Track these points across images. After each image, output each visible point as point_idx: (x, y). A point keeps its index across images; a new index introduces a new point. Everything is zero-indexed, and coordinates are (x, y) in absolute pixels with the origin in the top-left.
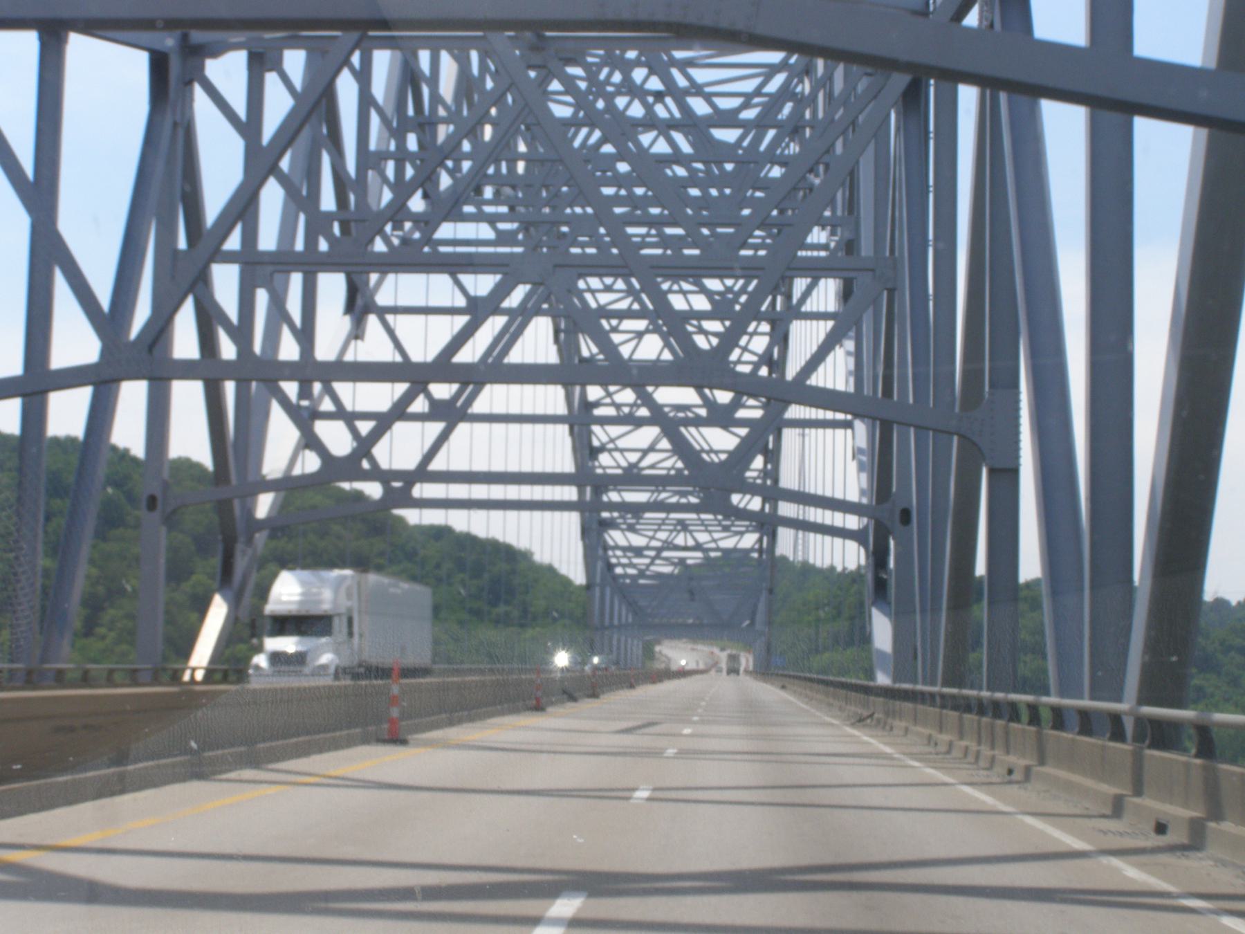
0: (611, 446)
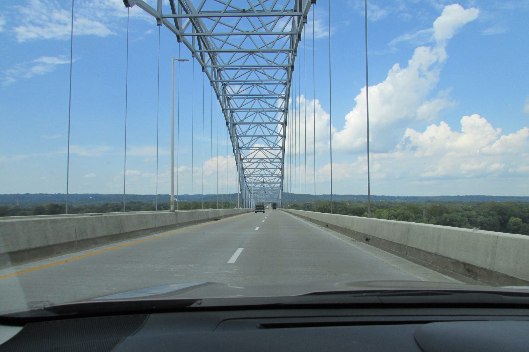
0: (246, 158)
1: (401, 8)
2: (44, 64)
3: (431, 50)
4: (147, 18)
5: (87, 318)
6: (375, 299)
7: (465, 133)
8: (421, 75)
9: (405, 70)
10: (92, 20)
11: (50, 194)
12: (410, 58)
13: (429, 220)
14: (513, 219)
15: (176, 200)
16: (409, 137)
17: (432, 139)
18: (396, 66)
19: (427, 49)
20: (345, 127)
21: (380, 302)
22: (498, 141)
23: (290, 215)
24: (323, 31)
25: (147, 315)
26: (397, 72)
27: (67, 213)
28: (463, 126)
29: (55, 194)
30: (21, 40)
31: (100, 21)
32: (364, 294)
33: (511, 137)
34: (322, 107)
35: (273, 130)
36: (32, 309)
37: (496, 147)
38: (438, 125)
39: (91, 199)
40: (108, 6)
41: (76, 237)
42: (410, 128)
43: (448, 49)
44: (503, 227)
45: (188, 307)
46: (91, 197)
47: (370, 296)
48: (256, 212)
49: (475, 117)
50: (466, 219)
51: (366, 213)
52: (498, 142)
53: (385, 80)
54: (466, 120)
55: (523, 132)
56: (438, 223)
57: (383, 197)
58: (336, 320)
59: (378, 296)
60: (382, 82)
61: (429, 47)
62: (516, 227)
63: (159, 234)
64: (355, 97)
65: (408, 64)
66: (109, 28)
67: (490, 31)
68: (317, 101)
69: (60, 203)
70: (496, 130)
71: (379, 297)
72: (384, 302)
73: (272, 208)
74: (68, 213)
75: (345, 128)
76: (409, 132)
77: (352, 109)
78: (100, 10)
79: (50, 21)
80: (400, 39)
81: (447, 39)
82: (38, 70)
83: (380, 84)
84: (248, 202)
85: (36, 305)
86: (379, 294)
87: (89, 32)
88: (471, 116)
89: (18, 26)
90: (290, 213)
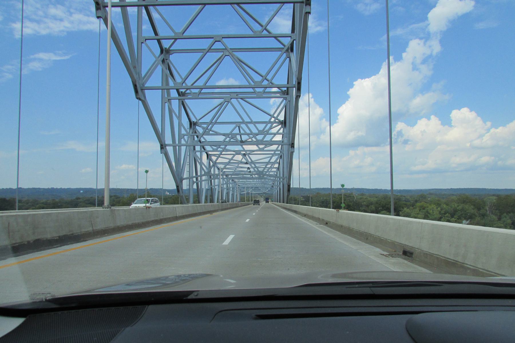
2: (40, 60)
3: (425, 44)
5: (88, 310)
6: (367, 291)
7: (455, 127)
8: (415, 68)
10: (88, 16)
12: (404, 51)
15: (167, 194)
16: (401, 130)
17: (423, 132)
20: (337, 121)
21: (372, 293)
22: (488, 134)
23: (292, 215)
25: (145, 307)
27: (17, 208)
32: (357, 286)
33: (500, 130)
34: (314, 101)
35: (264, 74)
36: (34, 301)
37: (487, 140)
38: (429, 119)
42: (401, 122)
43: (442, 42)
44: (471, 219)
45: (185, 298)
46: (81, 191)
47: (363, 287)
48: (254, 205)
53: (378, 73)
54: (456, 114)
58: (329, 311)
59: (370, 287)
61: (423, 41)
63: (60, 248)
64: (349, 90)
65: (402, 57)
67: (481, 26)
68: (311, 96)
69: (8, 197)
70: (485, 124)
71: (371, 288)
72: (376, 293)
73: (265, 201)
74: (19, 210)
75: (338, 122)
77: (344, 103)
79: (46, 16)
81: (441, 31)
83: (373, 77)
84: (233, 195)
85: (38, 297)
86: (371, 285)
87: (85, 28)
90: (295, 212)
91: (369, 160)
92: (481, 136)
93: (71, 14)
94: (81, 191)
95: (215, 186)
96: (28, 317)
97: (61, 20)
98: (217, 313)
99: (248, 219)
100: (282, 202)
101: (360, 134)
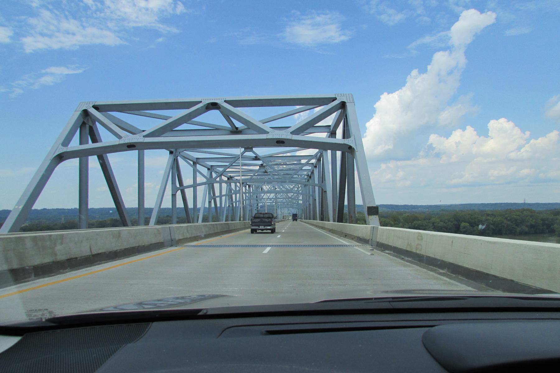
1: (419, 12)
2: (52, 74)
4: (159, 27)
7: (492, 138)
9: (424, 76)
10: (102, 29)
11: (67, 209)
13: (403, 226)
14: (463, 224)
17: (458, 144)
18: (414, 72)
19: (446, 53)
20: (365, 135)
21: (391, 307)
22: (527, 145)
24: (340, 35)
25: (150, 324)
26: (416, 78)
28: (490, 130)
29: (72, 209)
30: (28, 50)
31: (110, 29)
33: (541, 142)
37: (526, 151)
38: (464, 129)
39: (112, 213)
40: (120, 16)
41: (190, 213)
44: (457, 230)
46: (111, 212)
49: (502, 120)
50: (431, 225)
51: (359, 222)
52: (527, 148)
54: (493, 124)
55: (553, 135)
56: (410, 228)
57: (405, 206)
59: (389, 302)
60: (401, 89)
62: (464, 229)
64: (375, 104)
66: (119, 37)
67: (513, 32)
71: (391, 303)
76: (433, 138)
78: (112, 20)
79: (59, 31)
80: (419, 42)
82: (47, 80)
87: (98, 41)
88: (499, 120)
89: (25, 36)
91: (401, 174)
92: (519, 149)
93: (84, 27)
94: (111, 212)
95: (236, 202)
96: (24, 336)
97: (74, 34)
98: (225, 330)
99: (278, 238)
100: (318, 219)
101: (387, 147)
